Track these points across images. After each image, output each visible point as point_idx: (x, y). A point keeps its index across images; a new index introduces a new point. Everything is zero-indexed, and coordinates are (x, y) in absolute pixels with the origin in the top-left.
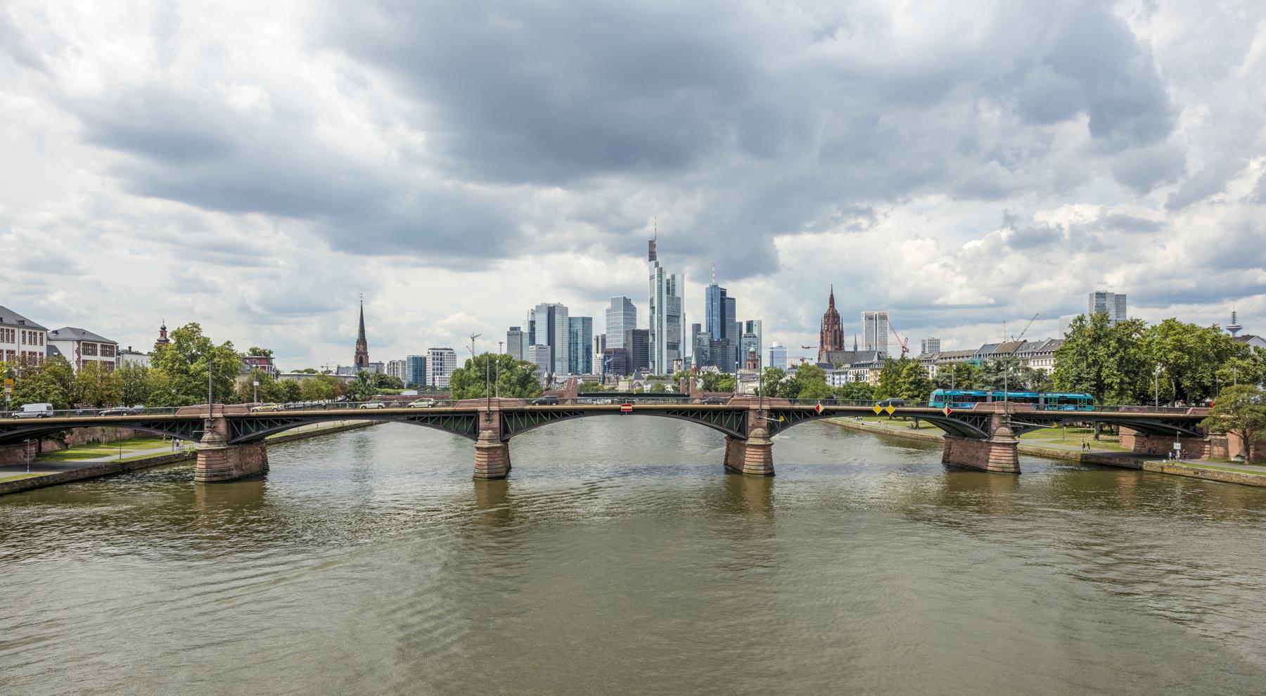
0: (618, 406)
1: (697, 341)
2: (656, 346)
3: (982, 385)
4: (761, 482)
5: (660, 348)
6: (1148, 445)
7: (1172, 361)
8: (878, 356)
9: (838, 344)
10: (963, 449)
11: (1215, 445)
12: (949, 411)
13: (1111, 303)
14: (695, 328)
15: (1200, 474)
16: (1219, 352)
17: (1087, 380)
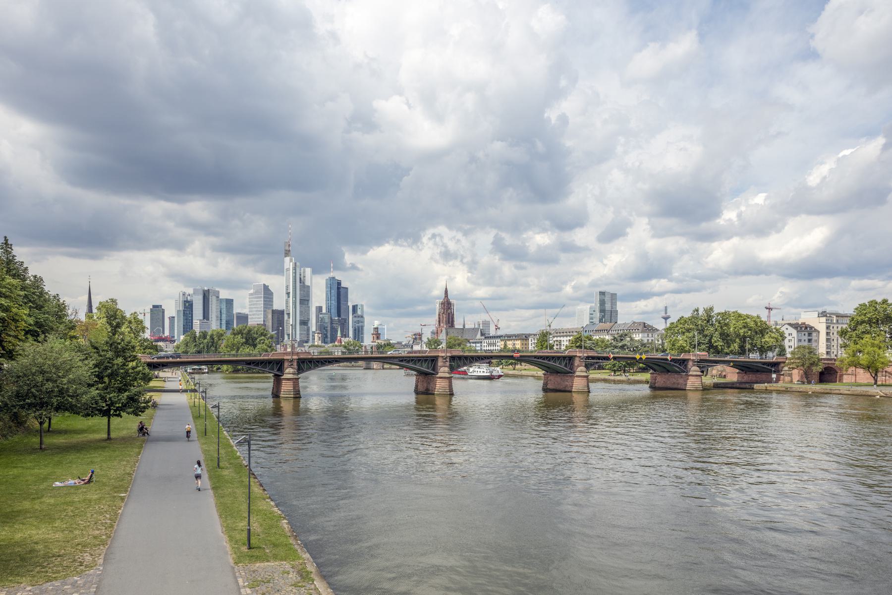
0: (512, 354)
1: (320, 319)
3: (612, 348)
4: (586, 395)
6: (746, 378)
7: (742, 334)
8: (481, 331)
9: (451, 323)
10: (555, 381)
11: (786, 376)
12: (670, 358)
13: (608, 299)
14: (318, 310)
15: (789, 389)
16: (762, 330)
17: (703, 344)
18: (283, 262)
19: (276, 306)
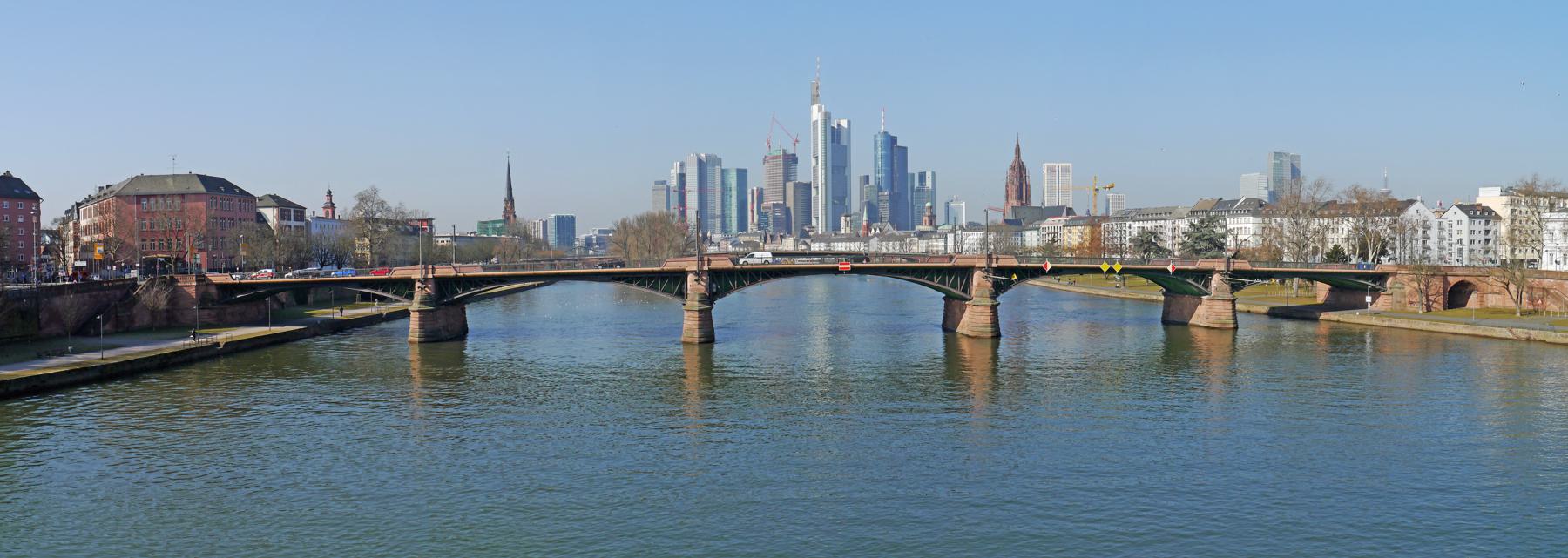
2: (820, 201)
5: (824, 202)
12: (1173, 267)
18: (810, 112)
19: (802, 177)
